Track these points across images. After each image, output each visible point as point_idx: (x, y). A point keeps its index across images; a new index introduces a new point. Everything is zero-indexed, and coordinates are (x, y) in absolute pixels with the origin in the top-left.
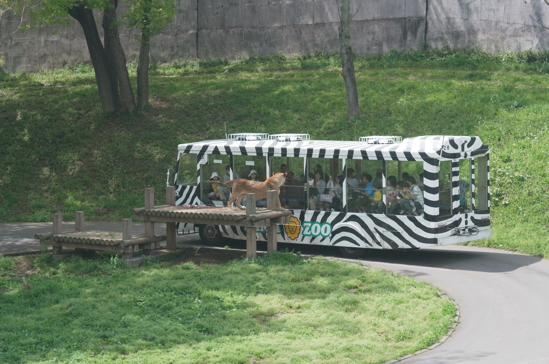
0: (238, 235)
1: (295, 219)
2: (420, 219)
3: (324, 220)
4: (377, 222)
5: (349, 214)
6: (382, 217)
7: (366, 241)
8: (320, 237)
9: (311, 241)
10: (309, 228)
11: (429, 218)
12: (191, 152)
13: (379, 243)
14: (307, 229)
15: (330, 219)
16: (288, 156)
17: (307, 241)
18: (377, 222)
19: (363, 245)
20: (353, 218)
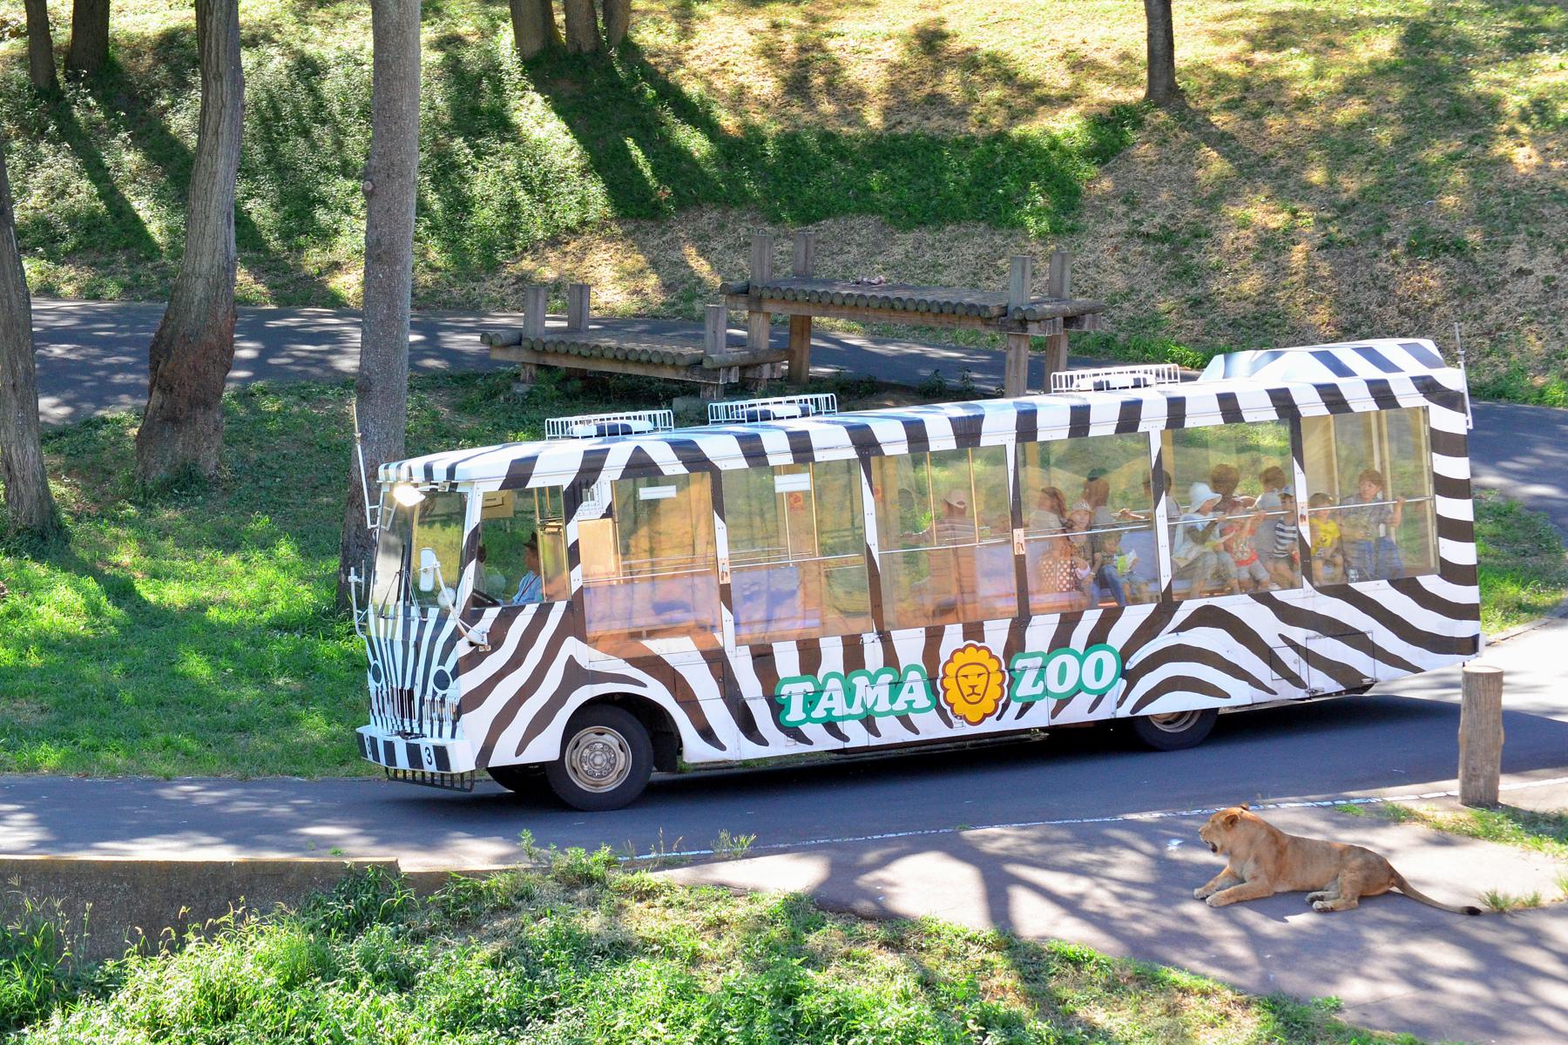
0: (763, 742)
1: (983, 652)
2: (1432, 583)
3: (1098, 637)
4: (1288, 614)
5: (1187, 609)
6: (1303, 597)
7: (1256, 683)
8: (1084, 700)
9: (1054, 714)
10: (1035, 672)
11: (1452, 572)
12: (533, 483)
13: (1295, 680)
14: (1029, 677)
15: (1120, 634)
16: (1041, 437)
17: (1038, 718)
18: (1288, 614)
19: (1240, 695)
20: (1209, 617)
